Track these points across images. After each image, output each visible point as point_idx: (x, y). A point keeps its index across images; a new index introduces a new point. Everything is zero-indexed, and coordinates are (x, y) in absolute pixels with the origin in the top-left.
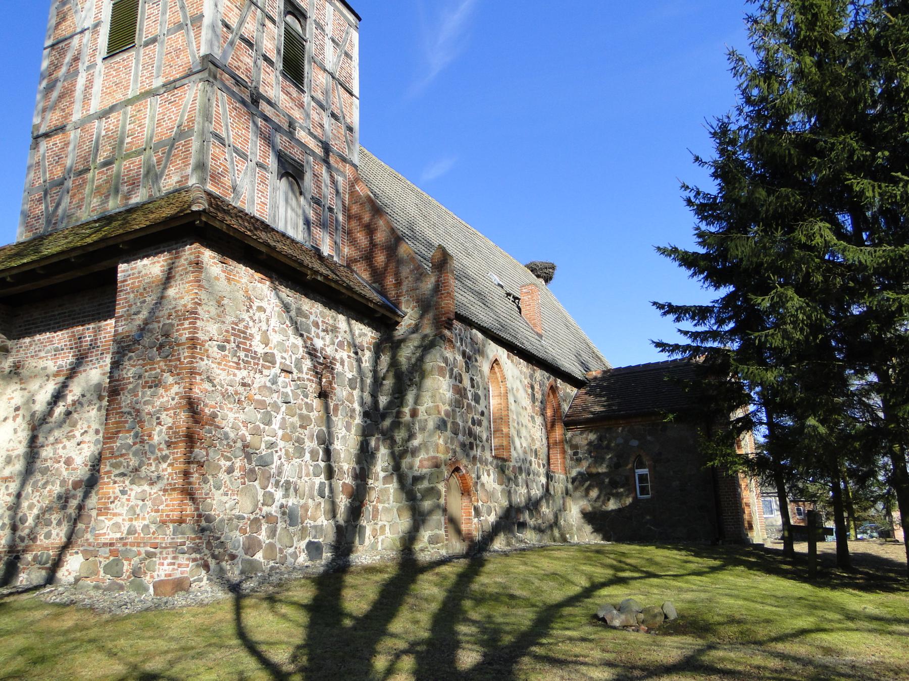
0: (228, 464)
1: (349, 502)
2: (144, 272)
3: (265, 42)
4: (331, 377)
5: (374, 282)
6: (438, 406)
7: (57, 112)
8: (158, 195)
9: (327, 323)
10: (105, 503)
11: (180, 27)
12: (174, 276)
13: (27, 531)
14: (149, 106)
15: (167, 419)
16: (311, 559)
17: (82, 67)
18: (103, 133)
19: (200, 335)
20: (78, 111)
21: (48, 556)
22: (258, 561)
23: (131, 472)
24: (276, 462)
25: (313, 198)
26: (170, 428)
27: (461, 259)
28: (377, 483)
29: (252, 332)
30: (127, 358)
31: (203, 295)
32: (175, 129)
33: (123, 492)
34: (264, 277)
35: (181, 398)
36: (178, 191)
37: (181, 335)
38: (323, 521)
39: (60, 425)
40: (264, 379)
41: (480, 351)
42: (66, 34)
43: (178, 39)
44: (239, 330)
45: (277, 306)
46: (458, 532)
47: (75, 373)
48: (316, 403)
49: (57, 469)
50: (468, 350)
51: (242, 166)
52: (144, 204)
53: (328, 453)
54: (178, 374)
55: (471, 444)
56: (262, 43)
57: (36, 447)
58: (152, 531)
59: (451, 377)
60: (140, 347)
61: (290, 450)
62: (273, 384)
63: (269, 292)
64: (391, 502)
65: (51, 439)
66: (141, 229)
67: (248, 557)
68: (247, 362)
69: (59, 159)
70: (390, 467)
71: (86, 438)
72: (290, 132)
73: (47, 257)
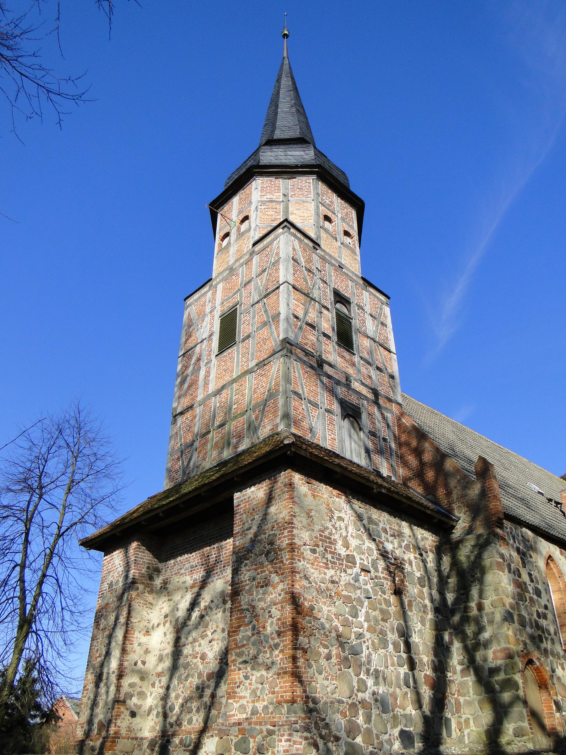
0: (326, 651)
1: (433, 694)
2: (252, 497)
3: (323, 324)
4: (402, 576)
5: (428, 495)
6: (502, 599)
7: (188, 396)
8: (257, 441)
9: (394, 529)
10: (233, 688)
11: (265, 324)
12: (274, 497)
13: (175, 718)
14: (247, 381)
15: (276, 612)
16: (405, 748)
17: (202, 364)
18: (218, 405)
19: (296, 541)
20: (201, 394)
21: (191, 738)
22: (359, 745)
23: (252, 659)
24: (365, 652)
25: (370, 432)
26: (279, 619)
27: (498, 470)
28: (455, 675)
29: (336, 538)
30: (243, 564)
31: (296, 509)
32: (266, 393)
33: (246, 677)
34: (340, 493)
35: (286, 593)
36: (272, 436)
37: (282, 542)
38: (411, 710)
39: (196, 627)
40: (348, 578)
41: (532, 548)
42: (192, 345)
43: (265, 332)
44: (325, 536)
45: (352, 516)
46: (542, 726)
47: (206, 583)
48: (393, 599)
49: (195, 664)
50: (521, 547)
51: (315, 413)
52: (248, 449)
53: (408, 645)
54: (282, 574)
55: (540, 636)
56: (321, 324)
57: (179, 646)
58: (270, 711)
59: (510, 571)
60: (253, 555)
61: (375, 641)
62: (356, 582)
63: (345, 505)
64: (471, 695)
65: (190, 639)
66: (250, 463)
67: (350, 740)
68: (334, 563)
69: (189, 428)
70: (466, 660)
71: (216, 636)
72: (347, 384)
73: (186, 494)
